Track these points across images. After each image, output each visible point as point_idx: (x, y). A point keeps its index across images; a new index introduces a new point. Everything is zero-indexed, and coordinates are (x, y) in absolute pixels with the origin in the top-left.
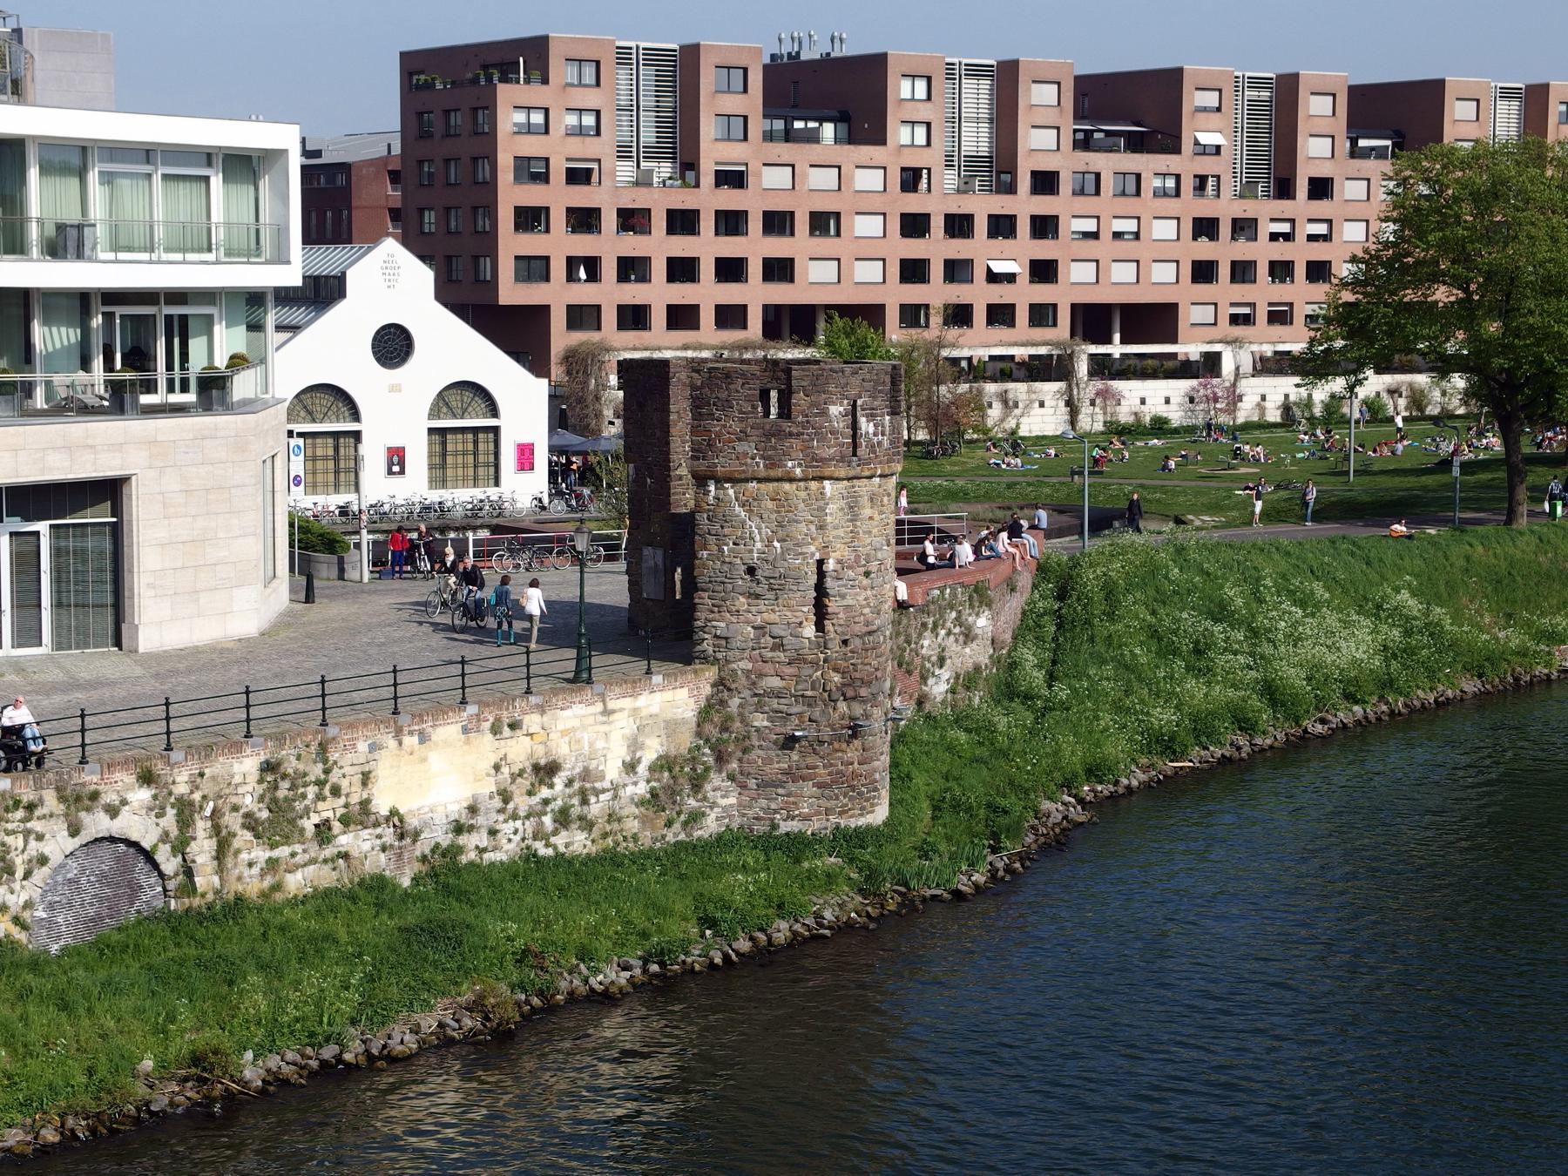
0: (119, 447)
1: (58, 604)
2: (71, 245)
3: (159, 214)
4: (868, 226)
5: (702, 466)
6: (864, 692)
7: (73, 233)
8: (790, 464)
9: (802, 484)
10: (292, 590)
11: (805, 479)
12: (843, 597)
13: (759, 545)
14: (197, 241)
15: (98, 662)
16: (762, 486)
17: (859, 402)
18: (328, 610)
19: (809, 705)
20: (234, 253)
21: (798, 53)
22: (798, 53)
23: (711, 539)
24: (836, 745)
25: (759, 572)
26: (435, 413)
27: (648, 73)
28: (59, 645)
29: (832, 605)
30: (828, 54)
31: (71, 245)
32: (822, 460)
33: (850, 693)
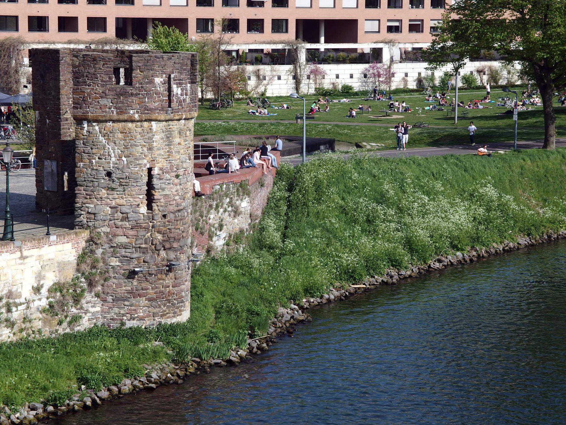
6: (175, 245)
17: (172, 76)
29: (157, 195)
33: (167, 246)
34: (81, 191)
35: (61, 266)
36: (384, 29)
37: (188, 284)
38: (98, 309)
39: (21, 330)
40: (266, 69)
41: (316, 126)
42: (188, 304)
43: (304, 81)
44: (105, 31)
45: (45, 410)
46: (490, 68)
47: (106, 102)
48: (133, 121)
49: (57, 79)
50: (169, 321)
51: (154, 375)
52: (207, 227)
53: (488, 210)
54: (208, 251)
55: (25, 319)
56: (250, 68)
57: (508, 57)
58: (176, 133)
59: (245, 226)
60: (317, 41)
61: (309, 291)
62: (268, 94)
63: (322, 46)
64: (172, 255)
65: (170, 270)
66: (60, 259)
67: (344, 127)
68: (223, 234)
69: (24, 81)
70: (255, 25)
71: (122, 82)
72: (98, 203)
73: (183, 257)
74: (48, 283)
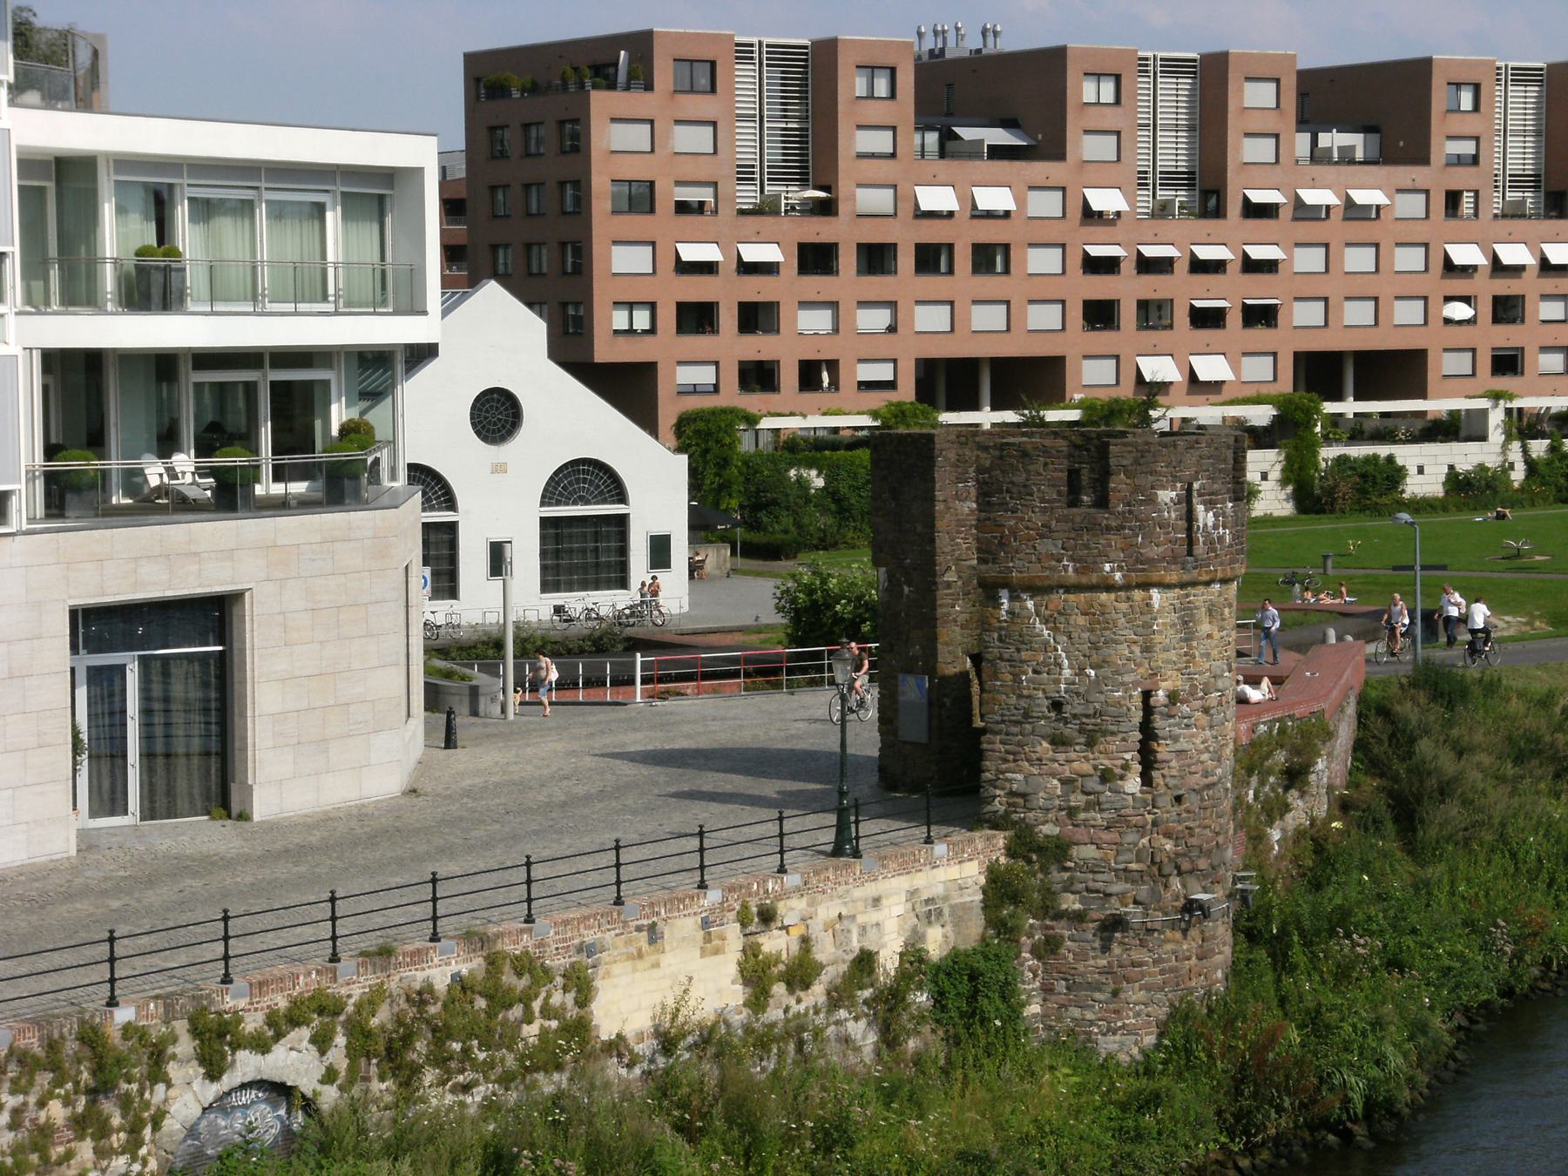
0: (229, 554)
1: (147, 755)
2: (156, 292)
3: (264, 253)
4: (1044, 261)
5: (991, 571)
6: (1203, 864)
7: (157, 278)
8: (1107, 567)
9: (1122, 594)
10: (428, 733)
11: (1127, 587)
12: (1175, 739)
13: (1067, 672)
14: (307, 287)
15: (196, 833)
16: (1071, 597)
17: (1196, 486)
18: (477, 760)
19: (1133, 882)
20: (351, 306)
21: (942, 50)
22: (942, 50)
23: (1004, 667)
24: (1169, 934)
25: (1067, 708)
26: (545, 501)
27: (772, 75)
28: (149, 813)
29: (1163, 750)
30: (979, 51)
31: (156, 292)
32: (1151, 561)
33: (1186, 866)
34: (994, 746)
60: (975, 406)
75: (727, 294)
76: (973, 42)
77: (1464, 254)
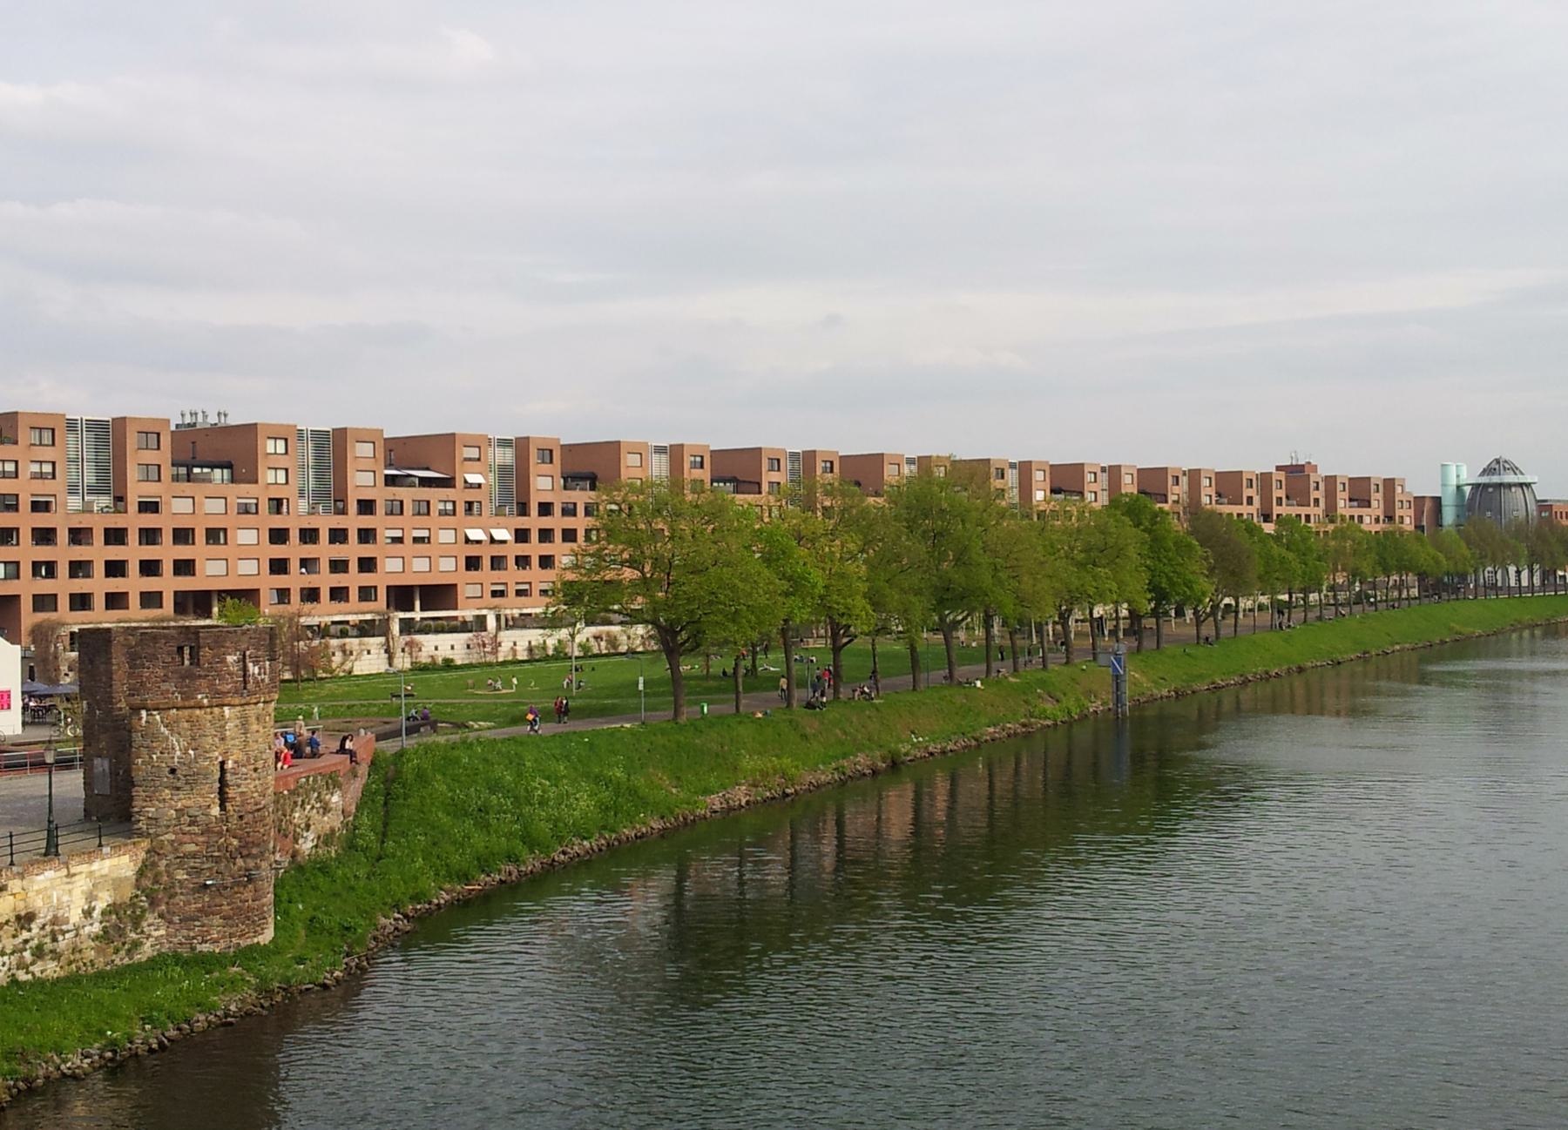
4: (246, 537)
6: (254, 851)
29: (231, 792)
33: (245, 852)
34: (139, 793)
35: (117, 883)
36: (488, 595)
37: (271, 896)
38: (162, 932)
39: (70, 963)
40: (353, 643)
41: (415, 705)
42: (271, 920)
43: (399, 654)
44: (161, 606)
45: (101, 1057)
46: (608, 634)
47: (169, 686)
48: (200, 708)
49: (109, 662)
50: (244, 943)
51: (233, 1008)
52: (291, 828)
53: (617, 795)
54: (293, 856)
55: (76, 950)
56: (334, 642)
57: (632, 618)
58: (253, 720)
59: (337, 825)
60: (412, 609)
61: (416, 898)
62: (356, 673)
63: (417, 615)
64: (251, 864)
65: (250, 880)
66: (114, 875)
67: (447, 705)
68: (311, 835)
69: (64, 668)
70: (339, 594)
71: (187, 663)
72: (159, 805)
73: (264, 865)
74: (100, 905)
75: (486, 553)
76: (212, 419)
77: (475, 534)
